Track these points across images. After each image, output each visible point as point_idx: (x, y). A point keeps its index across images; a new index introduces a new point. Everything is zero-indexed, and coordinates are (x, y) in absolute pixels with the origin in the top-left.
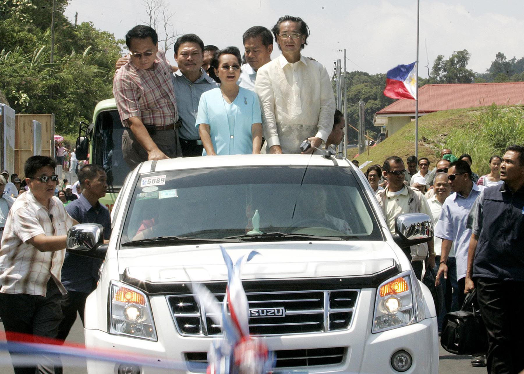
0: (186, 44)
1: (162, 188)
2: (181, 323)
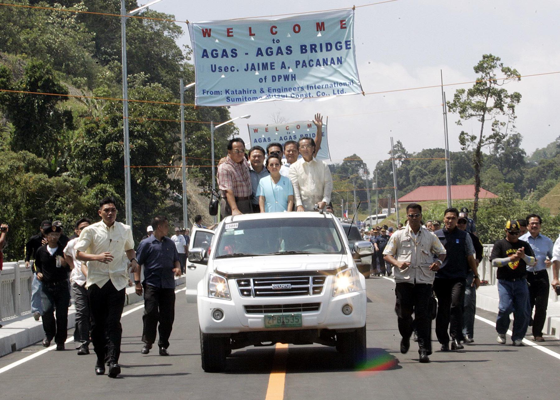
0: (255, 151)
1: (236, 229)
2: (242, 291)
